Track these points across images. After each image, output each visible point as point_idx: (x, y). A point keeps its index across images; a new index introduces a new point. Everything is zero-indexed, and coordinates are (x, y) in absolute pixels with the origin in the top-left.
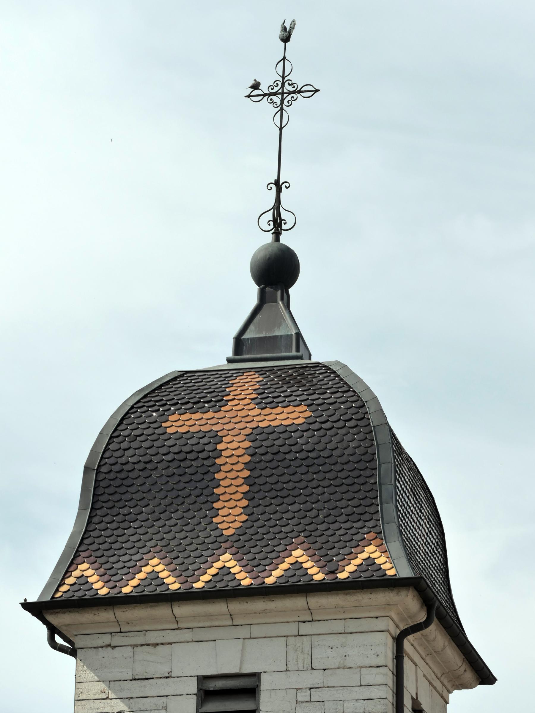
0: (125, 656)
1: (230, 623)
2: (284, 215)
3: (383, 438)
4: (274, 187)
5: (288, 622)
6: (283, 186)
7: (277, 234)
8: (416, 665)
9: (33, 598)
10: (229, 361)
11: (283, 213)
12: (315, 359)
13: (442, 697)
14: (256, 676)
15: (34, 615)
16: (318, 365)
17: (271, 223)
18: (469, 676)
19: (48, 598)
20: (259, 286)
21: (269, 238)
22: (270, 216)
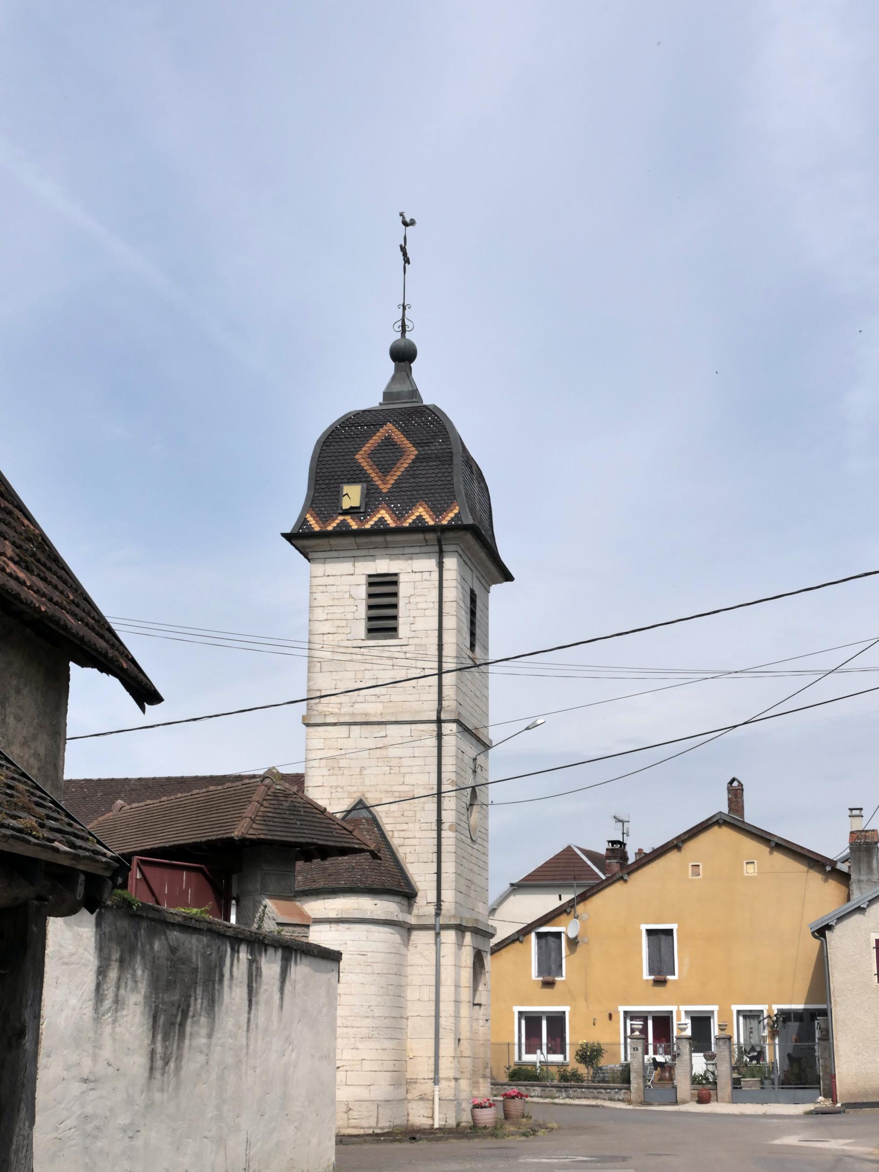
0: (186, 943)
1: (425, 544)
2: (407, 322)
3: (458, 450)
4: (402, 307)
5: (324, 551)
6: (407, 307)
7: (404, 331)
8: (472, 571)
9: (288, 530)
10: (380, 404)
11: (406, 321)
12: (425, 402)
13: (486, 589)
14: (396, 575)
15: (287, 540)
16: (425, 406)
17: (401, 327)
18: (500, 578)
19: (296, 532)
20: (384, 400)
21: (398, 336)
22: (400, 323)
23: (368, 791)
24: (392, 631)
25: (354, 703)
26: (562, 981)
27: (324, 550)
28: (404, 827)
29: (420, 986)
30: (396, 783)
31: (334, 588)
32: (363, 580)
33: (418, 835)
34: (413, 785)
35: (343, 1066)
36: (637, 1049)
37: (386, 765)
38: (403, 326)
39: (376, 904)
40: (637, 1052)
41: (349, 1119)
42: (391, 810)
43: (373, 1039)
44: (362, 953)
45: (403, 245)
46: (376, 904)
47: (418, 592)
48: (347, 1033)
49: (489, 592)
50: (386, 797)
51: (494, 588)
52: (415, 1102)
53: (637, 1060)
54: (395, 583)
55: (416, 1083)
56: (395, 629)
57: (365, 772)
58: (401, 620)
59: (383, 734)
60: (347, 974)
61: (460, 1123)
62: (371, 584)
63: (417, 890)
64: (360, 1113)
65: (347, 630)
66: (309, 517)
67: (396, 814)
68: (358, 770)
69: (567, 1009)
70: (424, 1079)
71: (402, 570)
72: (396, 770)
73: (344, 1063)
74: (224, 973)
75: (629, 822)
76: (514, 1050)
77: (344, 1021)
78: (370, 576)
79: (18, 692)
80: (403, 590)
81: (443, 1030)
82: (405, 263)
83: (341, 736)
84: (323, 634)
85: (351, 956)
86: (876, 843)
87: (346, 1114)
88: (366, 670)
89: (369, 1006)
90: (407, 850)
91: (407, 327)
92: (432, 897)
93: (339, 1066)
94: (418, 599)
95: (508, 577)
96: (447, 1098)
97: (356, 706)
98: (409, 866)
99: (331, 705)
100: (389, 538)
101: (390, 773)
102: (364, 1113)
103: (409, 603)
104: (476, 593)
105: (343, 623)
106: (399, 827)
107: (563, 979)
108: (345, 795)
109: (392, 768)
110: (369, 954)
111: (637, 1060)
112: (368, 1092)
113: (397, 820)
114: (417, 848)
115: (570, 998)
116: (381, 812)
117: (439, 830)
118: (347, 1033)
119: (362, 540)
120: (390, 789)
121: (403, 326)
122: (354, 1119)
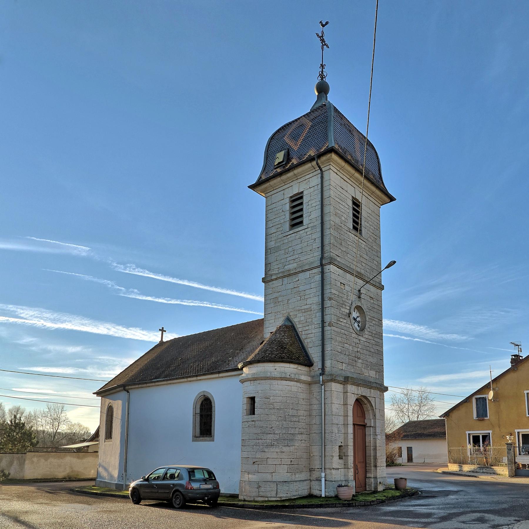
23: (291, 312)
25: (284, 266)
26: (487, 419)
27: (271, 191)
28: (307, 328)
29: (316, 416)
30: (303, 305)
31: (275, 209)
33: (313, 332)
34: (311, 304)
35: (256, 461)
36: (510, 450)
37: (299, 296)
39: (276, 369)
40: (510, 451)
41: (259, 492)
42: (301, 320)
43: (274, 446)
44: (267, 397)
46: (276, 369)
47: (312, 198)
48: (259, 443)
50: (299, 313)
52: (313, 481)
53: (510, 455)
55: (314, 470)
57: (290, 302)
59: (297, 279)
60: (258, 409)
63: (313, 362)
64: (265, 489)
65: (281, 229)
67: (303, 322)
68: (287, 301)
69: (490, 432)
70: (318, 468)
71: (305, 189)
72: (303, 297)
73: (257, 460)
75: (521, 345)
77: (257, 436)
78: (291, 197)
81: (327, 441)
83: (279, 285)
85: (261, 399)
87: (257, 489)
88: (289, 247)
89: (272, 428)
90: (309, 340)
92: (320, 366)
93: (255, 461)
94: (312, 202)
96: (329, 480)
97: (286, 267)
98: (309, 349)
99: (275, 270)
100: (296, 171)
101: (300, 300)
102: (268, 489)
103: (308, 205)
105: (279, 226)
106: (305, 329)
107: (488, 418)
108: (281, 315)
109: (301, 297)
110: (271, 398)
111: (510, 455)
112: (271, 476)
113: (304, 325)
114: (313, 338)
115: (492, 426)
116: (296, 322)
117: (323, 327)
118: (259, 443)
120: (300, 308)
122: (262, 492)
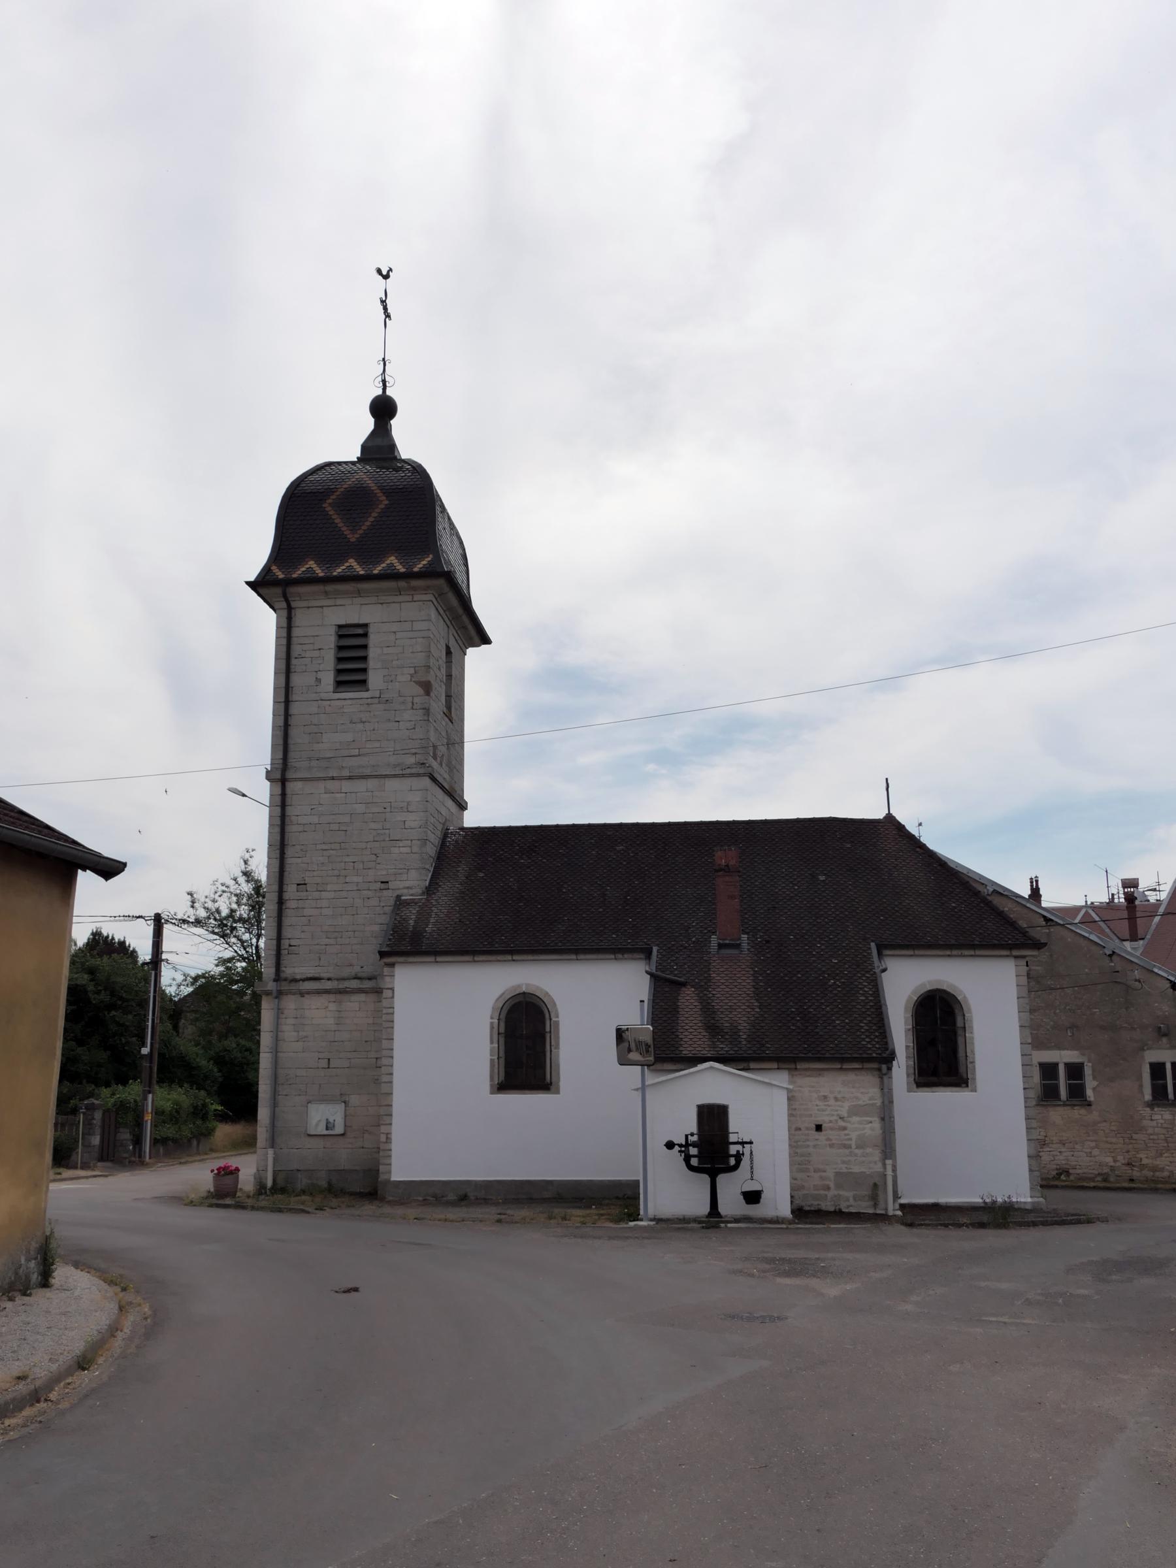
4: (382, 363)
9: (252, 578)
14: (366, 626)
18: (477, 639)
22: (380, 379)
24: (362, 683)
32: (332, 631)
38: (384, 382)
45: (387, 319)
49: (466, 655)
51: (471, 651)
54: (365, 635)
56: (363, 682)
58: (372, 663)
61: (401, 896)
62: (340, 637)
66: (274, 568)
74: (924, 1231)
75: (887, 779)
76: (148, 1032)
78: (340, 627)
79: (222, 962)
80: (373, 640)
82: (385, 301)
84: (331, 843)
86: (3, 1295)
91: (387, 383)
95: (486, 640)
104: (452, 650)
119: (330, 588)
121: (384, 382)
